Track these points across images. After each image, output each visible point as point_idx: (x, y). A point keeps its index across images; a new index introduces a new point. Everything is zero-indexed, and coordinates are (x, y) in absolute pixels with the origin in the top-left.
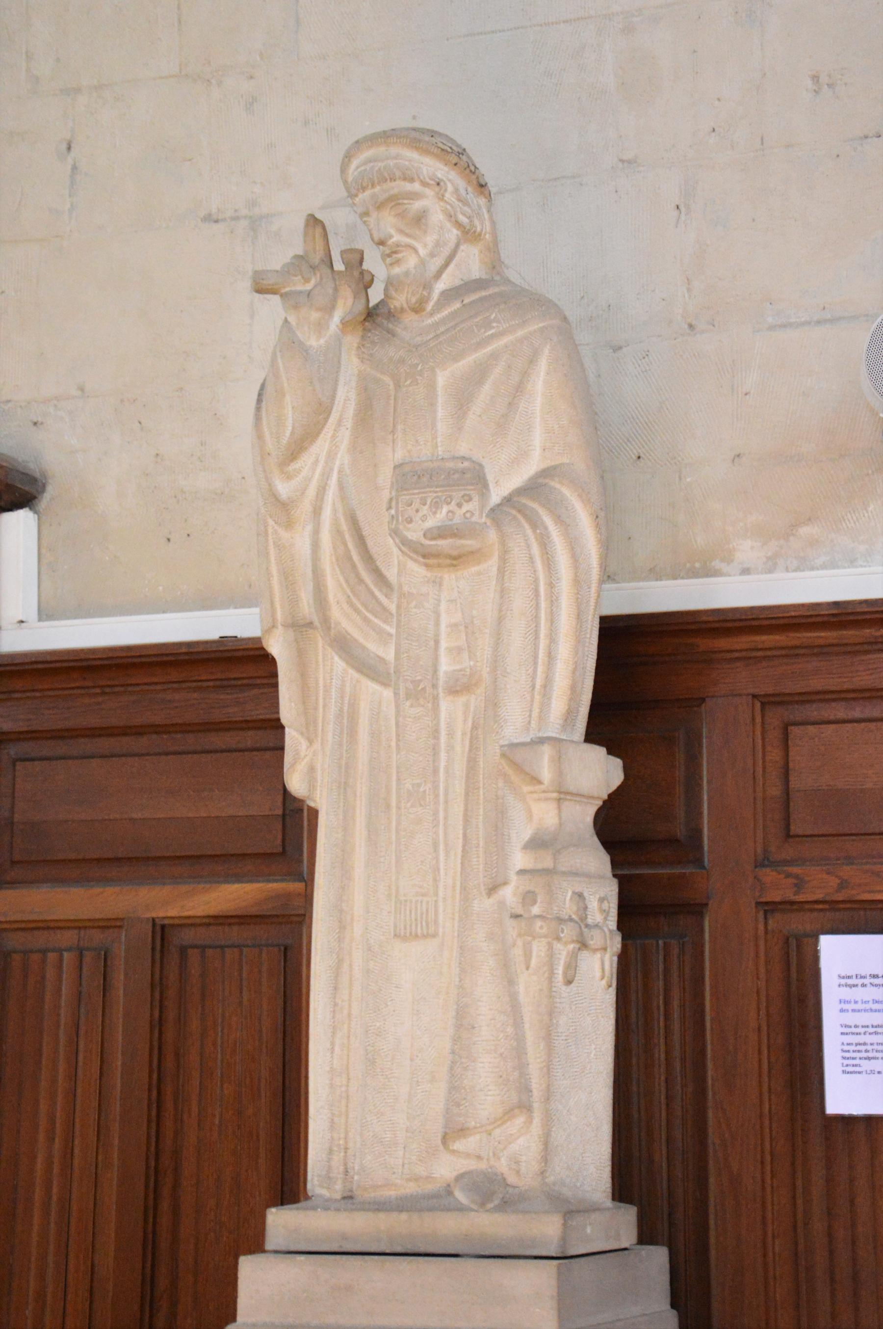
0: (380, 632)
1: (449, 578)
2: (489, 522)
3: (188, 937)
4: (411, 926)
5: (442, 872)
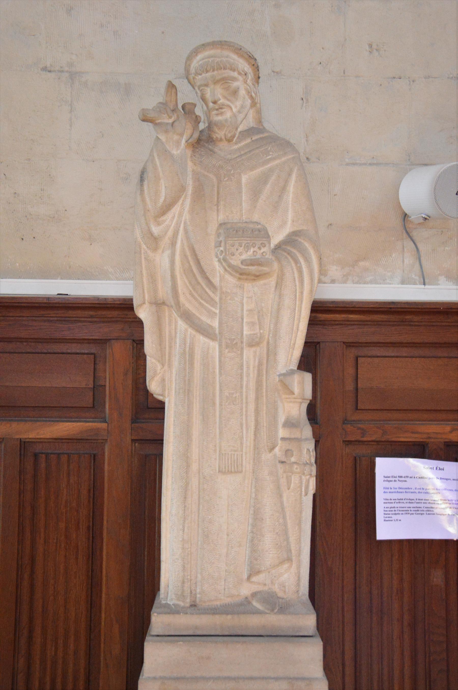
0: (209, 311)
1: (248, 286)
2: (273, 258)
3: (38, 448)
4: (228, 466)
5: (244, 439)
